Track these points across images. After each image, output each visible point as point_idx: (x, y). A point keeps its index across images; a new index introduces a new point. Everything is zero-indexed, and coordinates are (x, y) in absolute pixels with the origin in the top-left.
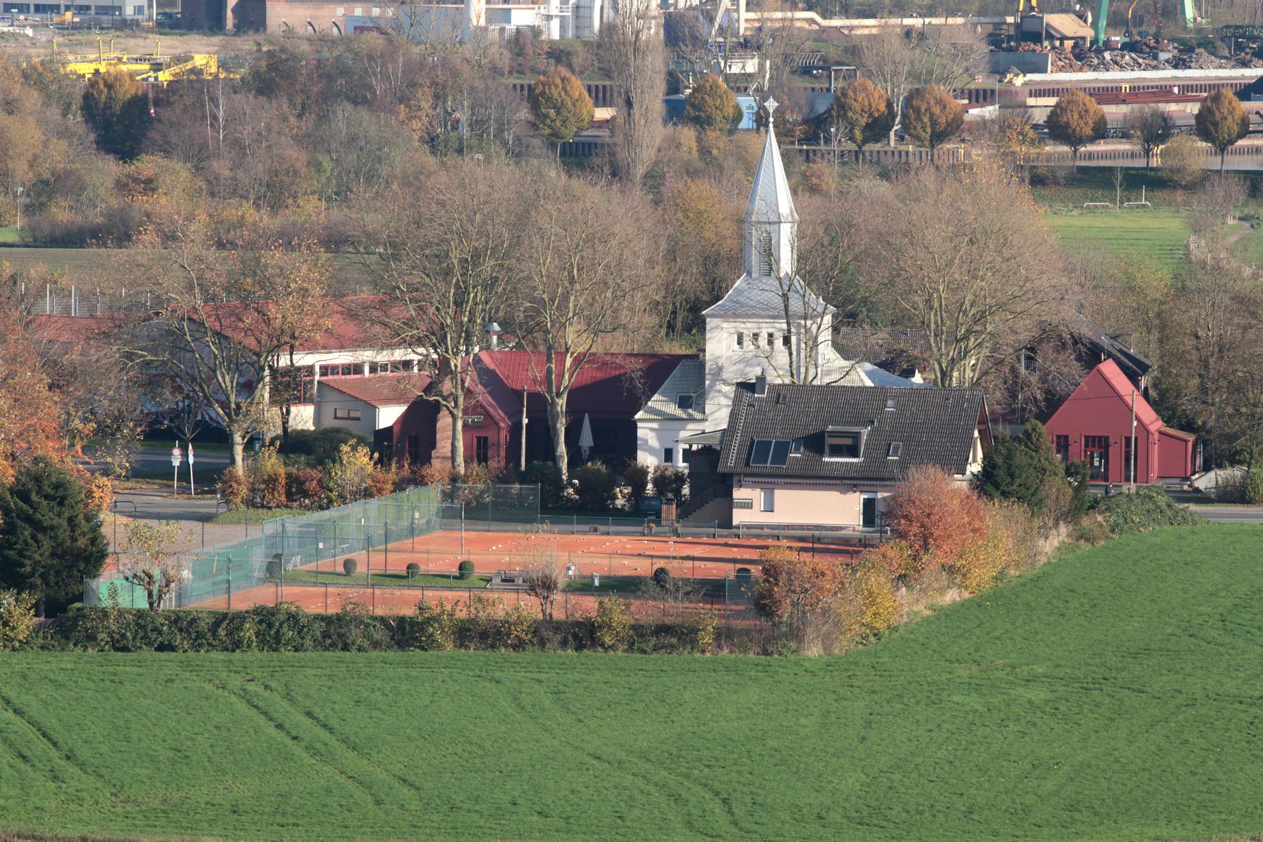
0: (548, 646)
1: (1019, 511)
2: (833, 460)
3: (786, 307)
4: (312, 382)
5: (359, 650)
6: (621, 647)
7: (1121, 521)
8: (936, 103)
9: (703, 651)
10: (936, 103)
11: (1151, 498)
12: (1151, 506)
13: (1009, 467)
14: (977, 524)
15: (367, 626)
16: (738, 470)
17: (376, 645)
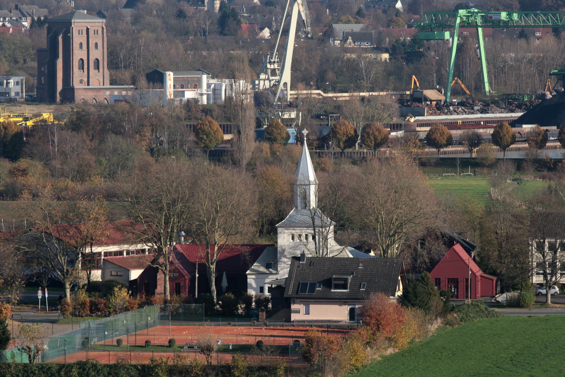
1: (420, 312)
2: (336, 291)
4: (100, 259)
7: (465, 316)
8: (376, 130)
10: (376, 130)
12: (478, 309)
14: (401, 319)
15: (128, 369)
16: (293, 296)
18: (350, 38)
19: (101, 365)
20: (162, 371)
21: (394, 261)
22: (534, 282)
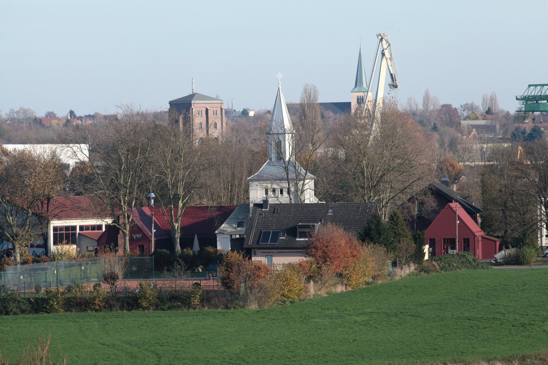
0: (114, 309)
1: (381, 250)
2: (301, 239)
4: (75, 234)
5: (14, 314)
6: (152, 308)
7: (447, 265)
8: (450, 166)
9: (195, 309)
10: (450, 166)
11: (464, 256)
12: (464, 260)
13: (378, 230)
14: (355, 253)
15: (19, 302)
16: (254, 246)
17: (23, 312)
18: (474, 130)
20: (58, 303)
22: (543, 245)
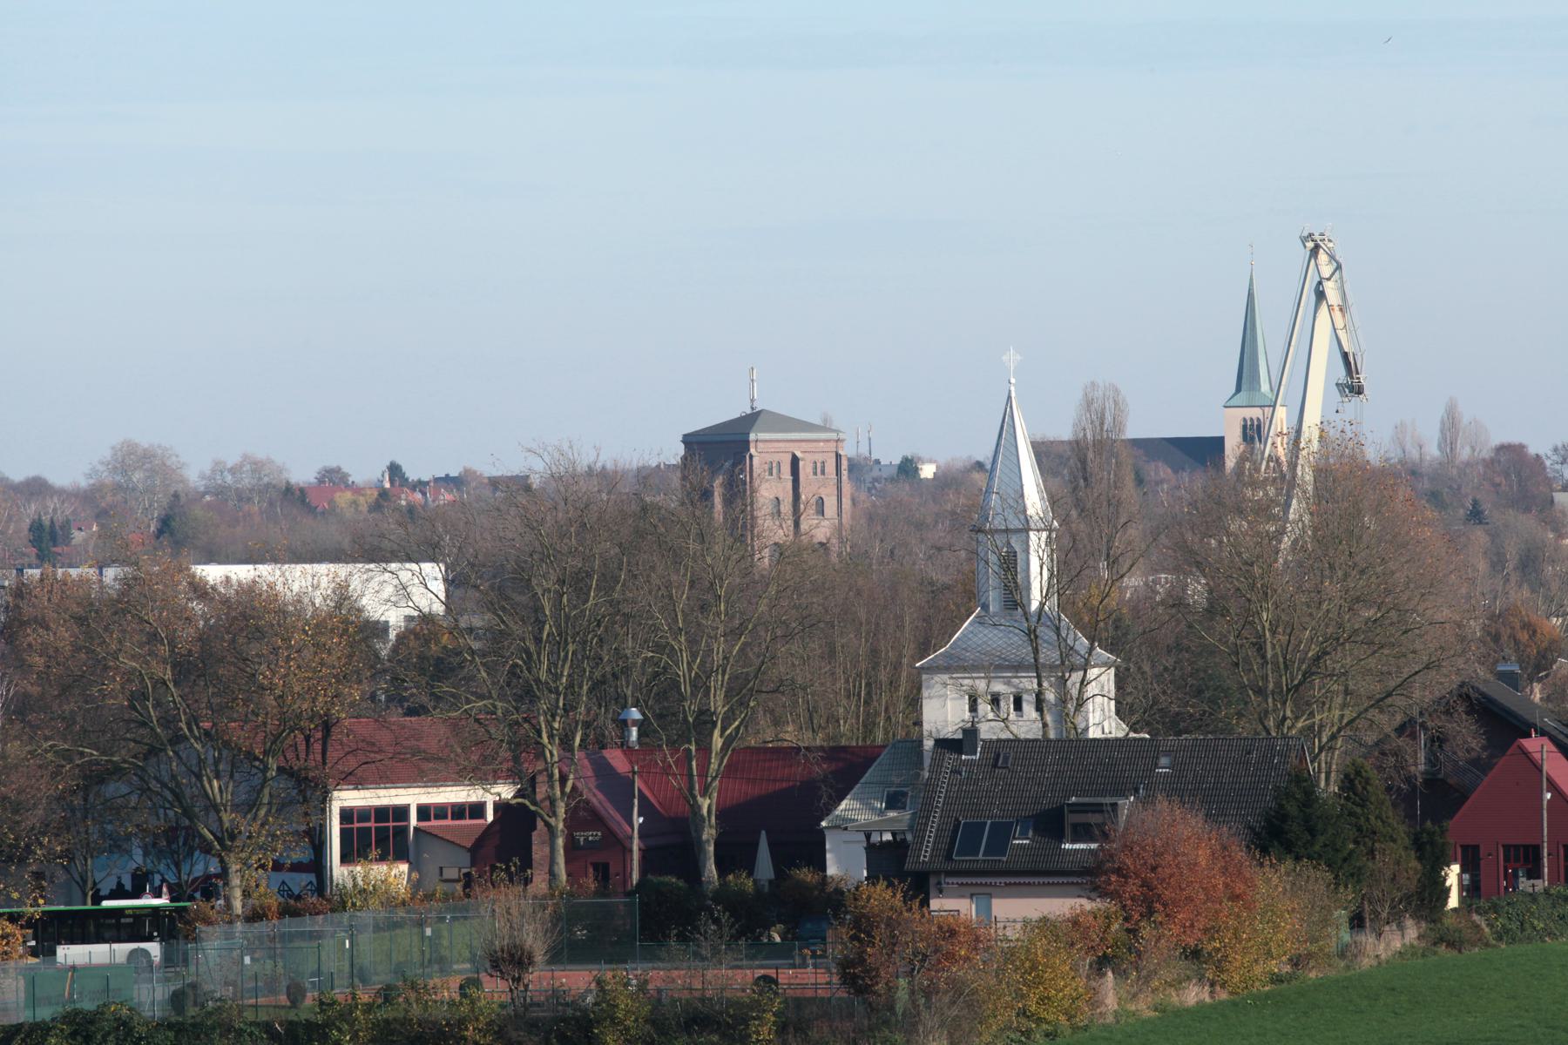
1: (1318, 878)
2: (1077, 846)
3: (1036, 660)
4: (406, 828)
8: (1523, 628)
10: (1523, 628)
14: (1240, 888)
16: (937, 866)
19: (147, 1024)
21: (1273, 747)
